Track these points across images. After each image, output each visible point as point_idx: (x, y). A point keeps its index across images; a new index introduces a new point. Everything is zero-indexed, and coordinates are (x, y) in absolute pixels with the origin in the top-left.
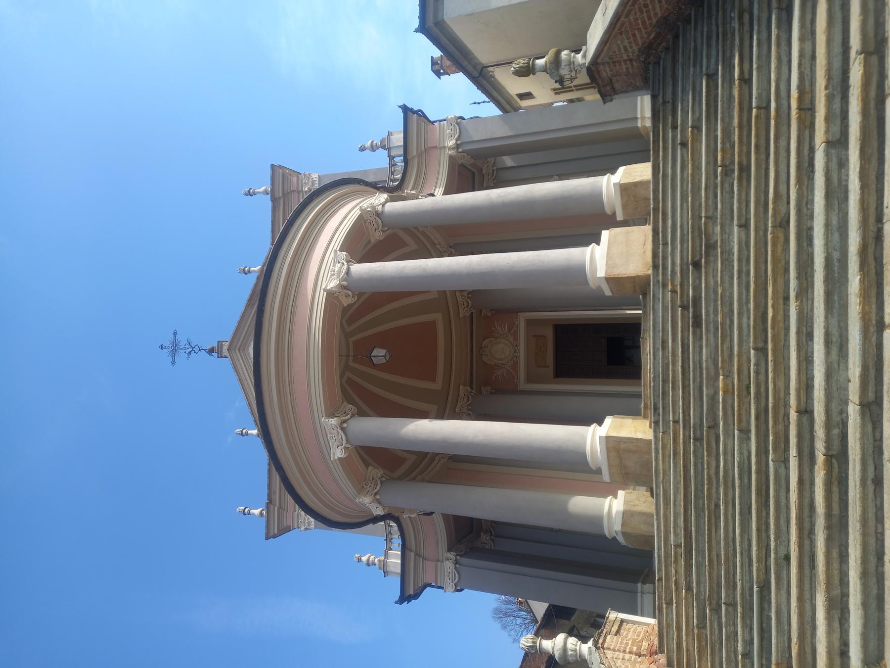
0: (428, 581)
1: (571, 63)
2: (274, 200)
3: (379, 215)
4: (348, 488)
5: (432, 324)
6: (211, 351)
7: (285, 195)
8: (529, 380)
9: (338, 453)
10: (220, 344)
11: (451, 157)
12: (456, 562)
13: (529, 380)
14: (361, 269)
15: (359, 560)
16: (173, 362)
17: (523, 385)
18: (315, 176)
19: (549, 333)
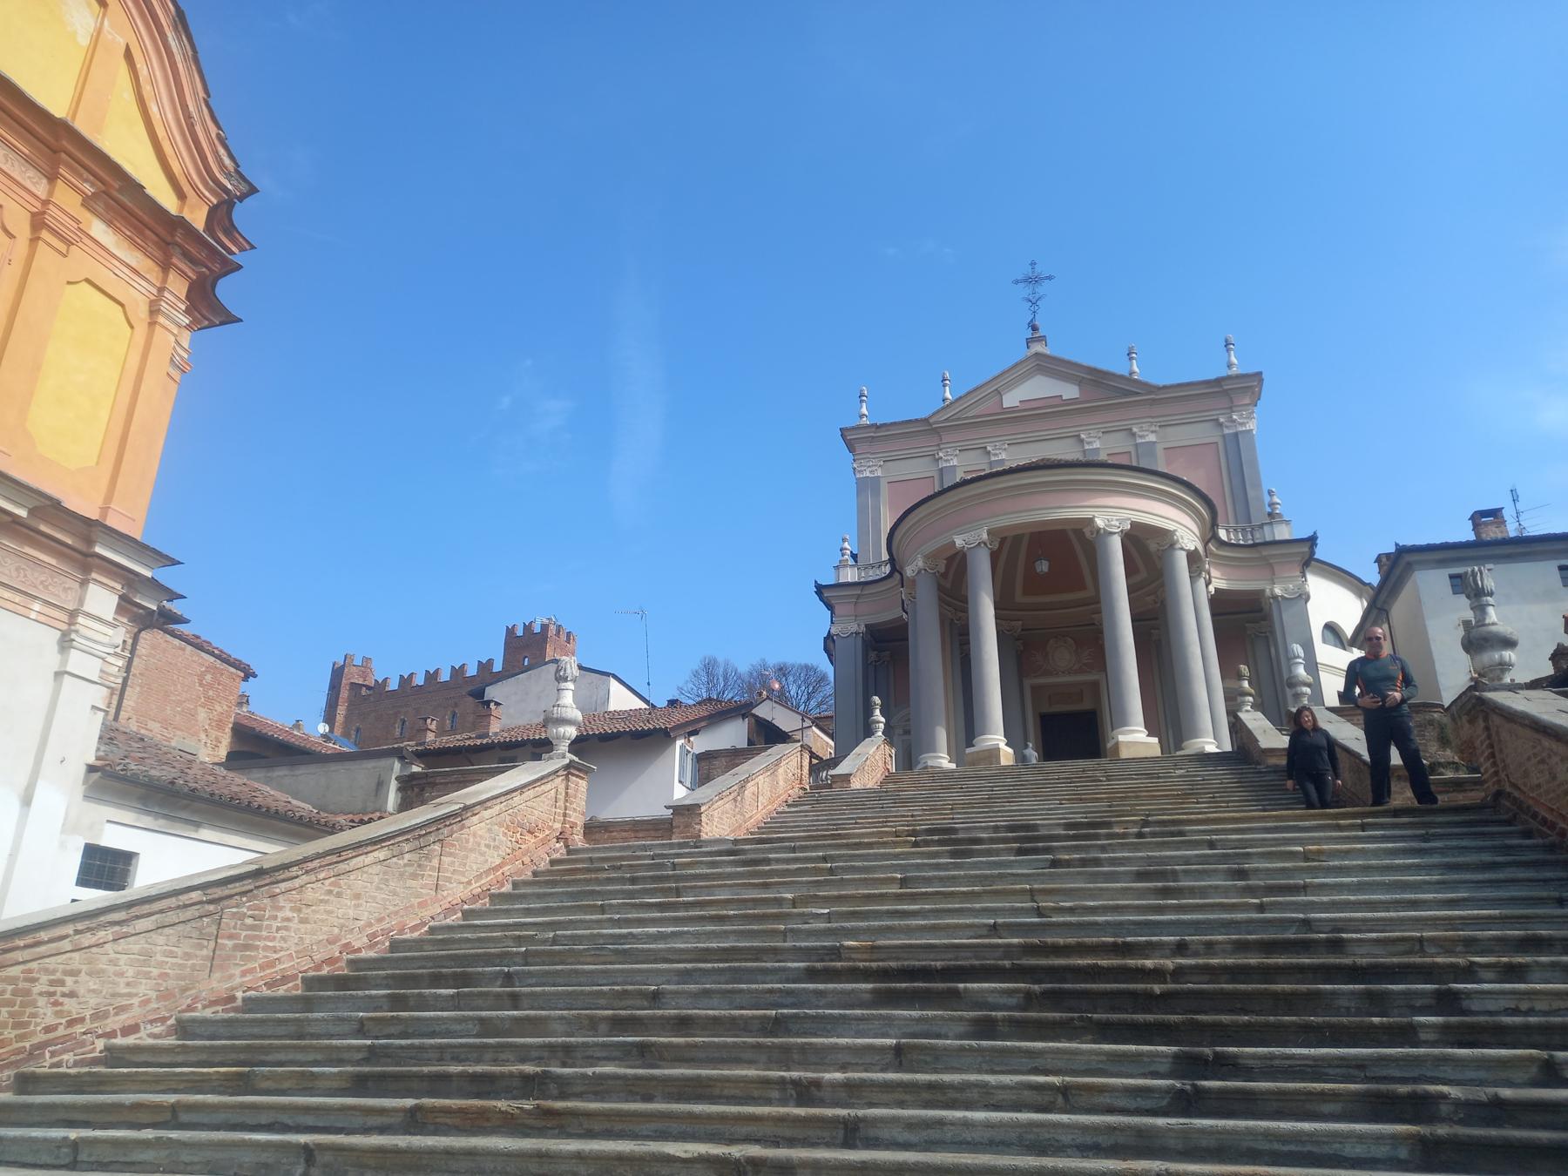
1: (1243, 703)
4: (930, 547)
5: (1083, 587)
6: (1035, 328)
7: (1226, 393)
9: (959, 542)
10: (1042, 339)
11: (1263, 591)
14: (1116, 546)
15: (844, 540)
16: (1017, 282)
17: (1028, 683)
18: (1252, 425)
19: (1086, 705)
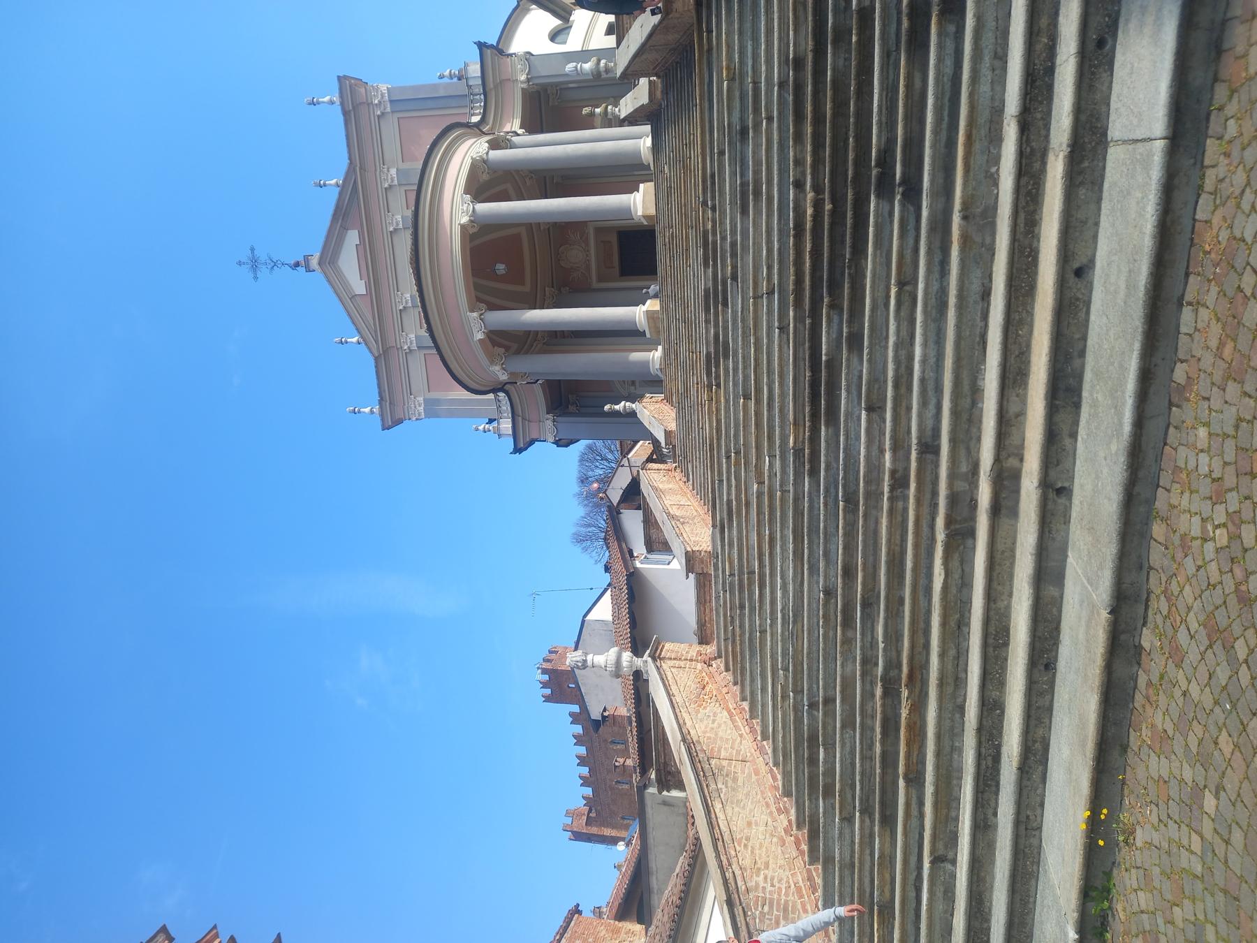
0: (534, 436)
2: (345, 113)
3: (485, 161)
6: (297, 265)
8: (600, 280)
9: (479, 336)
10: (306, 258)
12: (554, 421)
13: (600, 280)
14: (483, 207)
15: (477, 429)
17: (595, 285)
19: (614, 239)
